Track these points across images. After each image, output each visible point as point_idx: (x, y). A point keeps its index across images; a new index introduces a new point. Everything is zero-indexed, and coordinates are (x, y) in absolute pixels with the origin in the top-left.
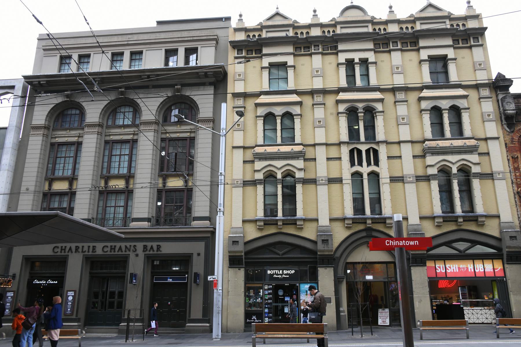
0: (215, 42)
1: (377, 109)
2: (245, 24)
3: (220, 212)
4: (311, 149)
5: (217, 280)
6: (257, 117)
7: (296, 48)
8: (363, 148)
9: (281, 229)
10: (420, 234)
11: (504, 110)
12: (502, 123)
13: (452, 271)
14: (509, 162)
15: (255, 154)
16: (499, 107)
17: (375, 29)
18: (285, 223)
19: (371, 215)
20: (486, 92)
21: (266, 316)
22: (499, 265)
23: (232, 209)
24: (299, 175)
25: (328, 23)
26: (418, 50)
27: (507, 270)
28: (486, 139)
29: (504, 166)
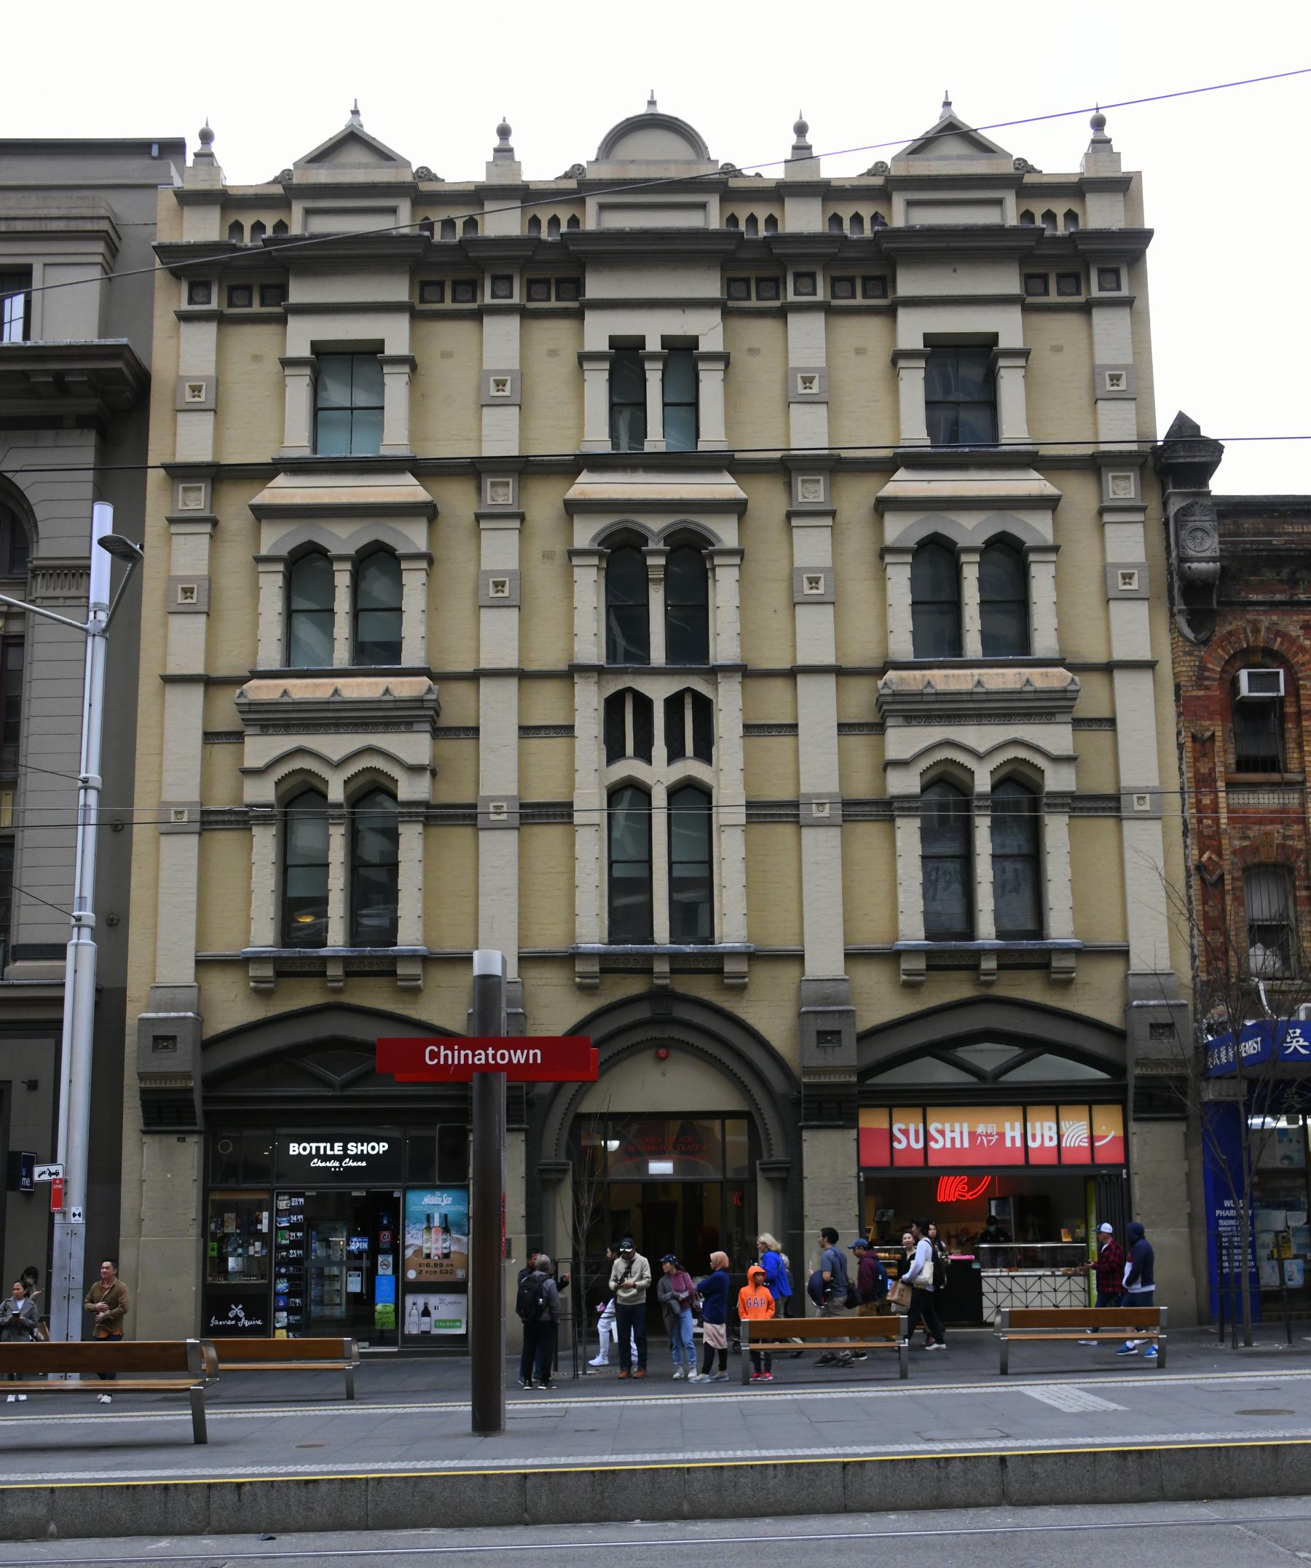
0: (100, 247)
1: (719, 540)
2: (524, 168)
3: (79, 927)
4: (461, 691)
5: (65, 1182)
6: (259, 560)
7: (424, 285)
8: (658, 691)
9: (338, 991)
10: (837, 1015)
11: (1182, 560)
12: (1171, 609)
13: (948, 1145)
14: (1181, 753)
15: (246, 708)
16: (1168, 545)
17: (733, 220)
18: (356, 969)
19: (671, 943)
20: (1124, 488)
21: (281, 1304)
22: (1109, 1126)
23: (156, 915)
24: (411, 789)
25: (553, 186)
26: (890, 312)
27: (1134, 1141)
28: (1109, 668)
29: (1161, 769)
